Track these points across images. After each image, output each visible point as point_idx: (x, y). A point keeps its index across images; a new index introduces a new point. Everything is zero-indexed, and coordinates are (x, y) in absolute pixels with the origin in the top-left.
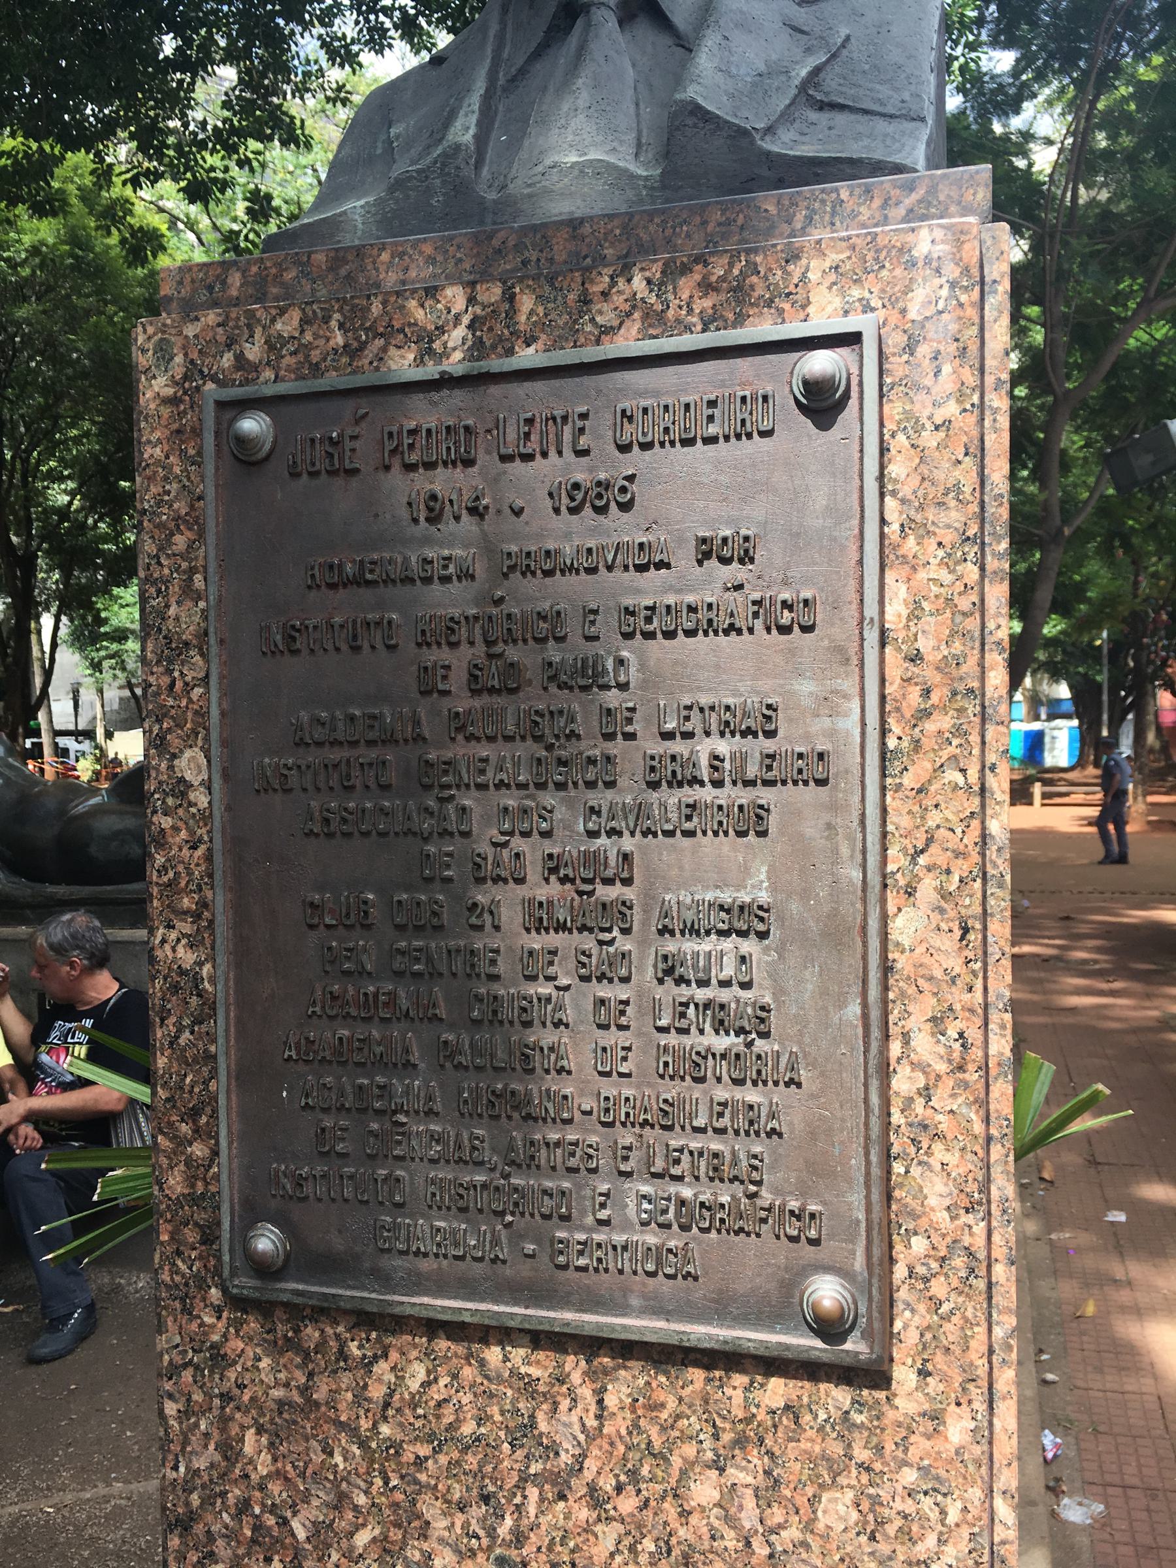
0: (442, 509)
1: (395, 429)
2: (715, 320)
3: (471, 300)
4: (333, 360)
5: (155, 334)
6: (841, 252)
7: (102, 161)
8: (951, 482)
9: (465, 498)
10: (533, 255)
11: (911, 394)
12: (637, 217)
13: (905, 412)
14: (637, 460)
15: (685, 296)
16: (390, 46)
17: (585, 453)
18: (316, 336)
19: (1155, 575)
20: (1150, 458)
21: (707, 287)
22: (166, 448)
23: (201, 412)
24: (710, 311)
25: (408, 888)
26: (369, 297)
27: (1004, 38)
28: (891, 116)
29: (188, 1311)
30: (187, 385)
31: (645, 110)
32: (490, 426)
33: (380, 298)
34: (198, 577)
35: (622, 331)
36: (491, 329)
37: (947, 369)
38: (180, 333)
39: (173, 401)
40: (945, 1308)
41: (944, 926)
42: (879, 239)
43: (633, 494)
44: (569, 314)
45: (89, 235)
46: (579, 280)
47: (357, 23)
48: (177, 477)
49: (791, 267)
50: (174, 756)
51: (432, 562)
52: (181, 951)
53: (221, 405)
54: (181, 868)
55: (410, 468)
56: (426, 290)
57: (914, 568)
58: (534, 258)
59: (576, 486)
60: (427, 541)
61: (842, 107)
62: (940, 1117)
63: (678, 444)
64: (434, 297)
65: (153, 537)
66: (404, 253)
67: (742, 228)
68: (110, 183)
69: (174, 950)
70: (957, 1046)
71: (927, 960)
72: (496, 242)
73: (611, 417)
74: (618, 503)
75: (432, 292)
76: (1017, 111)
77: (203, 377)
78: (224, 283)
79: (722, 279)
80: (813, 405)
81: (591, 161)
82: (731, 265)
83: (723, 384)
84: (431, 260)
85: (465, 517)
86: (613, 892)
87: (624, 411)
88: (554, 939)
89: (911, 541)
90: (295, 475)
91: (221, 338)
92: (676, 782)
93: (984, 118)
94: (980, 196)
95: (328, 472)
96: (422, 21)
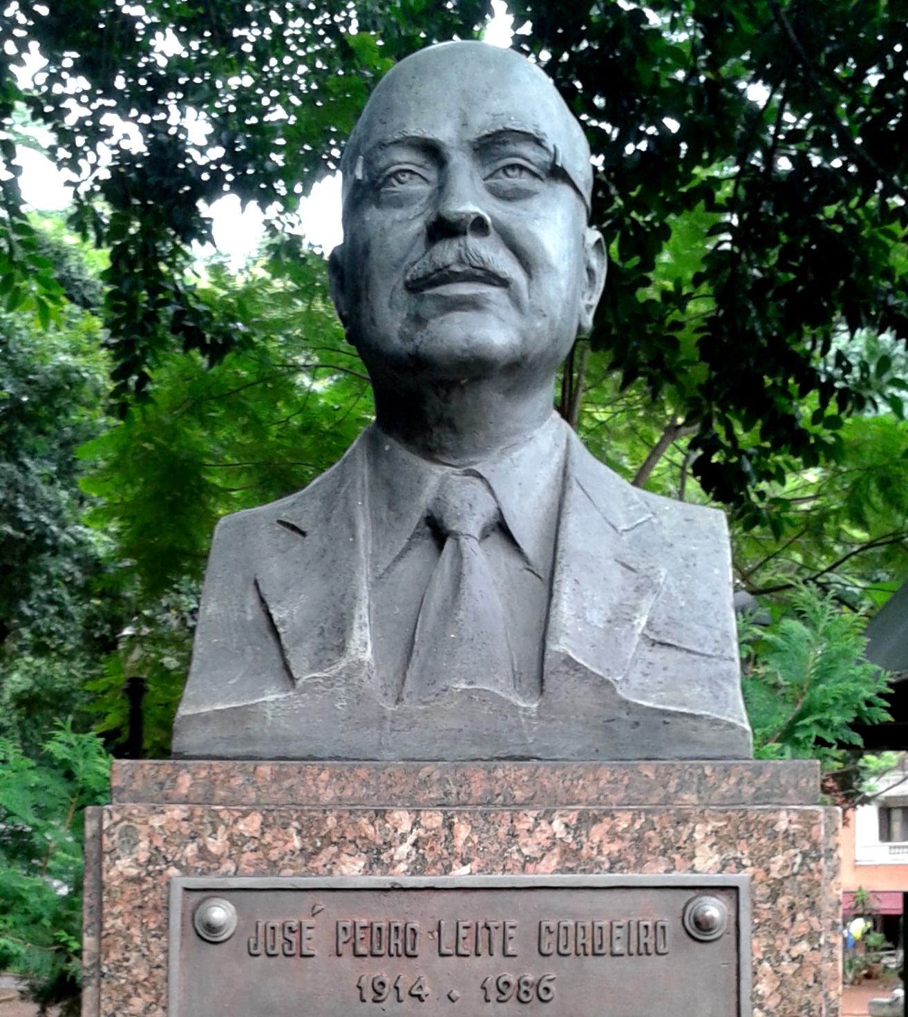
1: (349, 924)
3: (416, 824)
6: (720, 821)
11: (774, 932)
15: (596, 840)
18: (275, 838)
21: (613, 835)
26: (324, 812)
33: (335, 813)
35: (544, 861)
36: (432, 849)
37: (800, 917)
38: (146, 823)
42: (749, 814)
44: (500, 843)
46: (509, 818)
48: (137, 946)
49: (681, 828)
56: (377, 812)
58: (454, 792)
64: (383, 817)
67: (627, 787)
72: (422, 775)
79: (626, 830)
82: (633, 821)
84: (365, 783)
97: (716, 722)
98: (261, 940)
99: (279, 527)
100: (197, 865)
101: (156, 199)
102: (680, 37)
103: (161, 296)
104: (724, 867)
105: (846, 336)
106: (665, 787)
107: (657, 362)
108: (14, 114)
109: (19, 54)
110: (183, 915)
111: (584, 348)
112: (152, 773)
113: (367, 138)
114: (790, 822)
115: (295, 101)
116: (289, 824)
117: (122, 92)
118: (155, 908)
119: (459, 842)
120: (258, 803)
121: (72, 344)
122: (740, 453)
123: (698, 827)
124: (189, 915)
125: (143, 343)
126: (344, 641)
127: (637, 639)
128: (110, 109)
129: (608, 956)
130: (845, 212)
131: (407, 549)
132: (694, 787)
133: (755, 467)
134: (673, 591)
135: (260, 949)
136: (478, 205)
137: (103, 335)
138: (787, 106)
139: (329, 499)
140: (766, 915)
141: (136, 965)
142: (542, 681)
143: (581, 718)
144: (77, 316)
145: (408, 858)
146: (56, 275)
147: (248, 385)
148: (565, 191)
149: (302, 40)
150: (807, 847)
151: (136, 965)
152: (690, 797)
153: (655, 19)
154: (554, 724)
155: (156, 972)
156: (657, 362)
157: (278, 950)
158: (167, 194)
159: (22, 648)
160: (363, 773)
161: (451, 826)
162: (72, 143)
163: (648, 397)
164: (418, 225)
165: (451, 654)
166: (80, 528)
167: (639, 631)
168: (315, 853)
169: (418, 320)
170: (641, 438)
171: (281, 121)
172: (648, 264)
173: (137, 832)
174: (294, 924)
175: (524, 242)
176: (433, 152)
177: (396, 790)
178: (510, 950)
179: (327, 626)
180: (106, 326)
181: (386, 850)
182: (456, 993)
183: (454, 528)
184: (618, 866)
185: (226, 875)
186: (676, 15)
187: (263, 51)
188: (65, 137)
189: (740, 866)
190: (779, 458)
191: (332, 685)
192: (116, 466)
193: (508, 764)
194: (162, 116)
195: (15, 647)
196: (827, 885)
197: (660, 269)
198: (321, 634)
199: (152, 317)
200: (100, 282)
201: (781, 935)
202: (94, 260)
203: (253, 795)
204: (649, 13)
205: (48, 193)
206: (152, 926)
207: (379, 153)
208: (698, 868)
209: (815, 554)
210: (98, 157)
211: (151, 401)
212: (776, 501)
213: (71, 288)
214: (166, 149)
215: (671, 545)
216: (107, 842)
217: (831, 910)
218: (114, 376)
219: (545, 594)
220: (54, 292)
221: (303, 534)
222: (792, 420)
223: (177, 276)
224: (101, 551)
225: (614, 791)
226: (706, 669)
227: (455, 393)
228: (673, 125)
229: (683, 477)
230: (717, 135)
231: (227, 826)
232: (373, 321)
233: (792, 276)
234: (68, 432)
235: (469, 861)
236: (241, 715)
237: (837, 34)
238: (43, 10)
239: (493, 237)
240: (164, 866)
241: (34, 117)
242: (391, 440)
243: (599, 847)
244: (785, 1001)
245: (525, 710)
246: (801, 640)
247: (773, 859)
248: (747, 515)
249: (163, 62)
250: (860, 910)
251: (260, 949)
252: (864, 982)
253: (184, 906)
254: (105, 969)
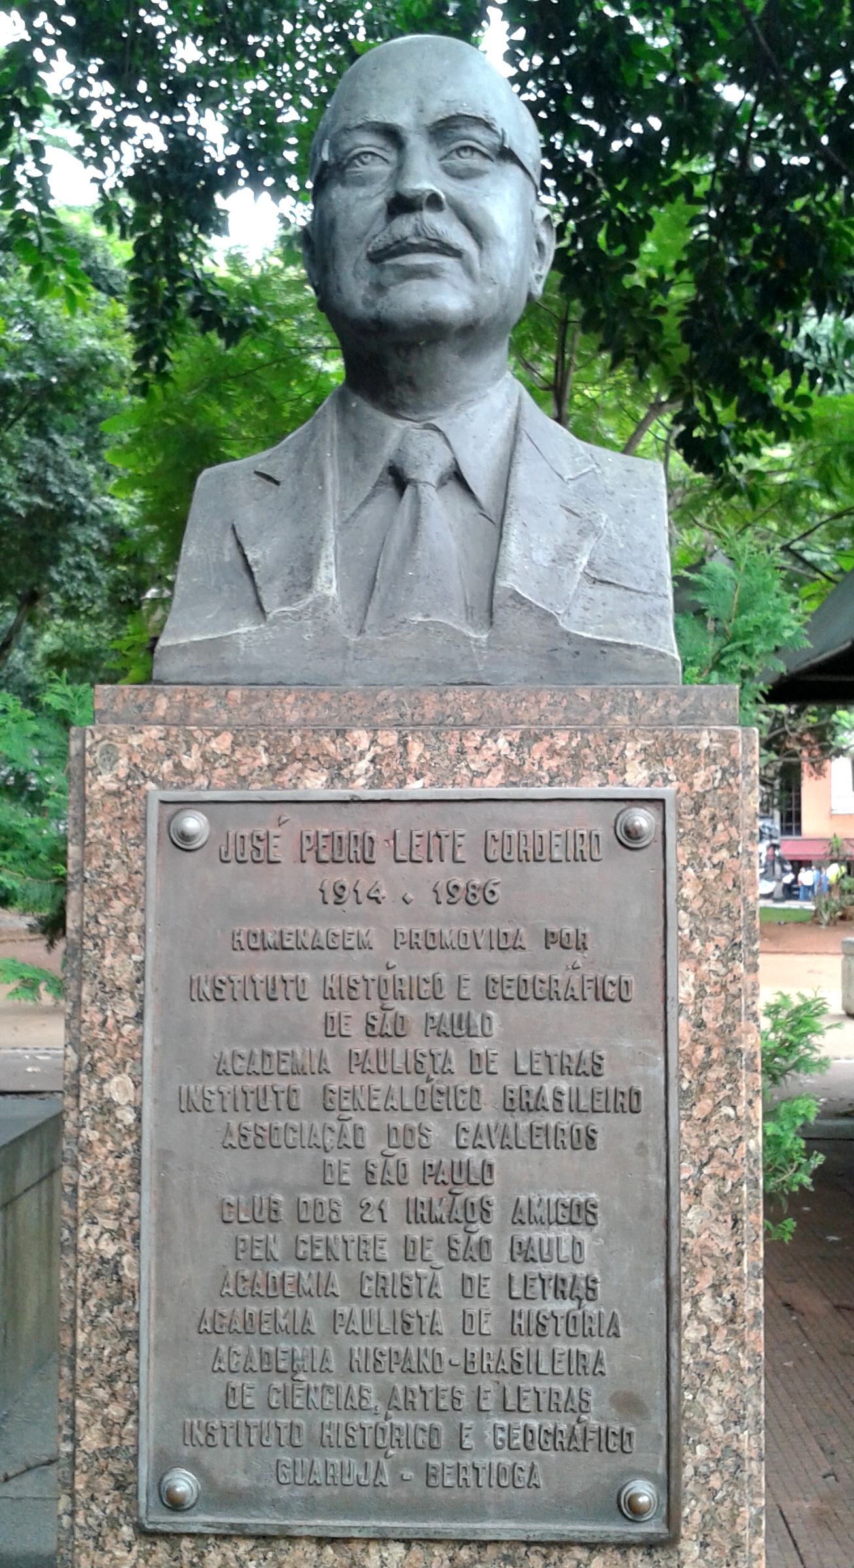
1: (312, 834)
3: (373, 742)
8: (724, 905)
15: (537, 757)
18: (245, 756)
21: (553, 752)
25: (311, 1189)
29: (99, 1547)
36: (388, 765)
37: (720, 827)
40: (719, 1496)
41: (721, 1218)
50: (104, 1081)
52: (102, 1245)
54: (106, 1174)
56: (338, 731)
57: (699, 962)
62: (717, 1357)
64: (343, 736)
69: (97, 1242)
70: (730, 1305)
71: (710, 1243)
72: (380, 698)
79: (564, 748)
82: (571, 739)
84: (328, 706)
86: (476, 1194)
88: (431, 1230)
89: (697, 943)
92: (528, 1109)
97: (648, 652)
98: (232, 847)
99: (255, 478)
101: (177, 192)
102: (661, 43)
103: (180, 284)
104: (652, 781)
105: (815, 320)
106: (599, 708)
107: (643, 343)
108: (43, 117)
109: (48, 61)
110: (159, 825)
111: (575, 331)
113: (334, 123)
115: (306, 103)
117: (144, 96)
118: (134, 819)
119: (413, 759)
120: (229, 724)
121: (98, 328)
122: (720, 428)
123: (629, 745)
124: (165, 825)
125: (164, 325)
127: (579, 577)
128: (133, 111)
129: (548, 862)
130: (813, 205)
131: (372, 496)
132: (626, 709)
133: (734, 441)
134: (614, 534)
135: (231, 856)
136: (432, 182)
137: (126, 320)
138: (760, 107)
139: (301, 452)
140: (689, 826)
142: (491, 615)
143: (527, 648)
144: (103, 303)
146: (83, 264)
147: (261, 365)
148: (514, 171)
149: (313, 47)
150: (726, 763)
152: (622, 718)
153: (638, 26)
154: (501, 654)
155: (134, 877)
156: (643, 343)
157: (247, 857)
158: (185, 189)
159: (53, 611)
160: (325, 697)
161: (405, 744)
162: (98, 143)
163: (634, 377)
164: (379, 202)
165: (410, 590)
166: (106, 499)
167: (581, 569)
168: (281, 769)
169: (380, 288)
170: (629, 415)
171: (294, 122)
172: (633, 253)
173: (118, 750)
174: (262, 834)
175: (475, 217)
176: (392, 135)
177: (356, 712)
178: (459, 856)
179: (297, 565)
180: (130, 312)
182: (410, 896)
184: (557, 780)
185: (199, 789)
186: (658, 22)
187: (275, 56)
188: (91, 137)
189: (666, 780)
190: (755, 433)
192: (138, 439)
193: (458, 689)
194: (179, 118)
195: (46, 610)
196: (745, 798)
197: (646, 258)
198: (291, 573)
199: (172, 302)
200: (125, 272)
201: (704, 843)
202: (119, 252)
203: (225, 717)
204: (633, 20)
205: (74, 187)
206: (131, 835)
207: (344, 137)
208: (628, 782)
209: (789, 523)
210: (122, 154)
211: (172, 380)
212: (753, 473)
213: (97, 277)
214: (185, 149)
215: (612, 493)
216: (89, 759)
217: (748, 821)
218: (136, 357)
219: (497, 536)
220: (80, 281)
221: (277, 483)
222: (765, 398)
223: (197, 265)
224: (126, 520)
225: (553, 713)
226: (641, 604)
227: (414, 354)
228: (655, 123)
229: (666, 450)
230: (696, 132)
232: (339, 290)
233: (765, 264)
234: (95, 410)
235: (423, 775)
236: (215, 646)
237: (804, 40)
238: (70, 21)
239: (447, 211)
241: (62, 119)
242: (358, 398)
245: (476, 640)
246: (725, 577)
248: (727, 485)
249: (182, 69)
250: (835, 855)
251: (231, 856)
252: (839, 923)
253: (160, 817)
254: (87, 875)
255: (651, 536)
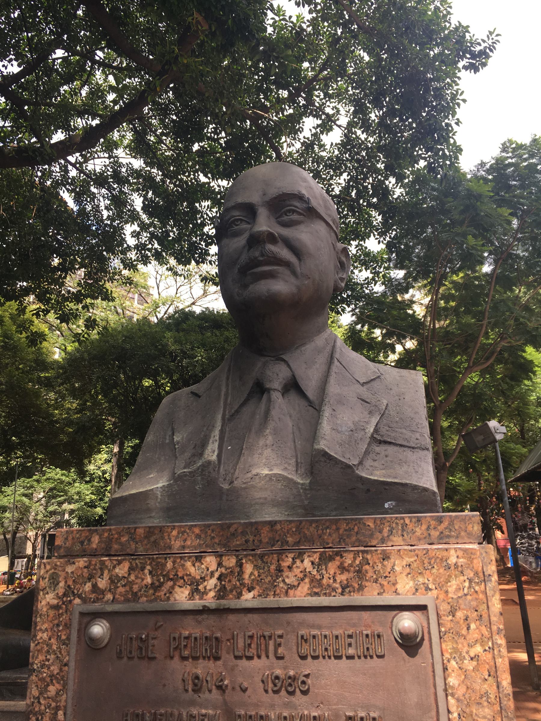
0: (201, 686)
1: (177, 636)
2: (348, 587)
3: (220, 565)
4: (145, 591)
5: (50, 569)
6: (411, 557)
7: (22, 305)
8: (483, 691)
9: (215, 678)
10: (251, 538)
11: (456, 638)
12: (304, 523)
13: (453, 648)
14: (309, 667)
15: (332, 572)
16: (150, 263)
17: (282, 658)
18: (137, 577)
19: (487, 480)
20: (482, 437)
21: (343, 569)
22: (50, 634)
23: (71, 614)
24: (345, 582)
26: (166, 558)
27: (399, 266)
28: (413, 448)
30: (65, 599)
31: (298, 443)
32: (229, 637)
33: (172, 559)
34: (61, 713)
35: (299, 588)
37: (473, 626)
38: (64, 570)
39: (56, 607)
42: (430, 552)
43: (309, 686)
44: (271, 576)
45: (12, 333)
46: (276, 558)
47: (137, 254)
48: (54, 651)
49: (386, 563)
51: (195, 717)
53: (82, 614)
55: (184, 659)
58: (251, 539)
59: (277, 678)
60: (192, 703)
61: (390, 443)
63: (332, 658)
64: (200, 561)
65: (37, 686)
66: (185, 532)
67: (357, 533)
68: (24, 313)
72: (232, 530)
73: (295, 638)
74: (300, 690)
75: (199, 559)
76: (407, 293)
77: (74, 595)
78: (89, 540)
79: (351, 565)
80: (406, 644)
81: (275, 474)
82: (355, 558)
83: (354, 625)
84: (198, 536)
85: (214, 690)
87: (302, 637)
90: (120, 657)
91: (86, 574)
93: (394, 294)
94: (476, 528)
95: (139, 658)
96: (164, 254)
100: (91, 596)
106: (381, 532)
112: (78, 536)
114: (458, 557)
116: (145, 567)
119: (246, 576)
126: (203, 451)
141: (53, 664)
145: (215, 588)
150: (472, 575)
151: (53, 664)
167: (369, 435)
181: (202, 583)
183: (268, 386)
184: (347, 590)
191: (194, 476)
201: (461, 640)
208: (400, 591)
221: (199, 397)
231: (109, 571)
239: (280, 244)
240: (72, 598)
243: (334, 577)
244: (470, 691)
247: (449, 584)
255: (416, 413)
